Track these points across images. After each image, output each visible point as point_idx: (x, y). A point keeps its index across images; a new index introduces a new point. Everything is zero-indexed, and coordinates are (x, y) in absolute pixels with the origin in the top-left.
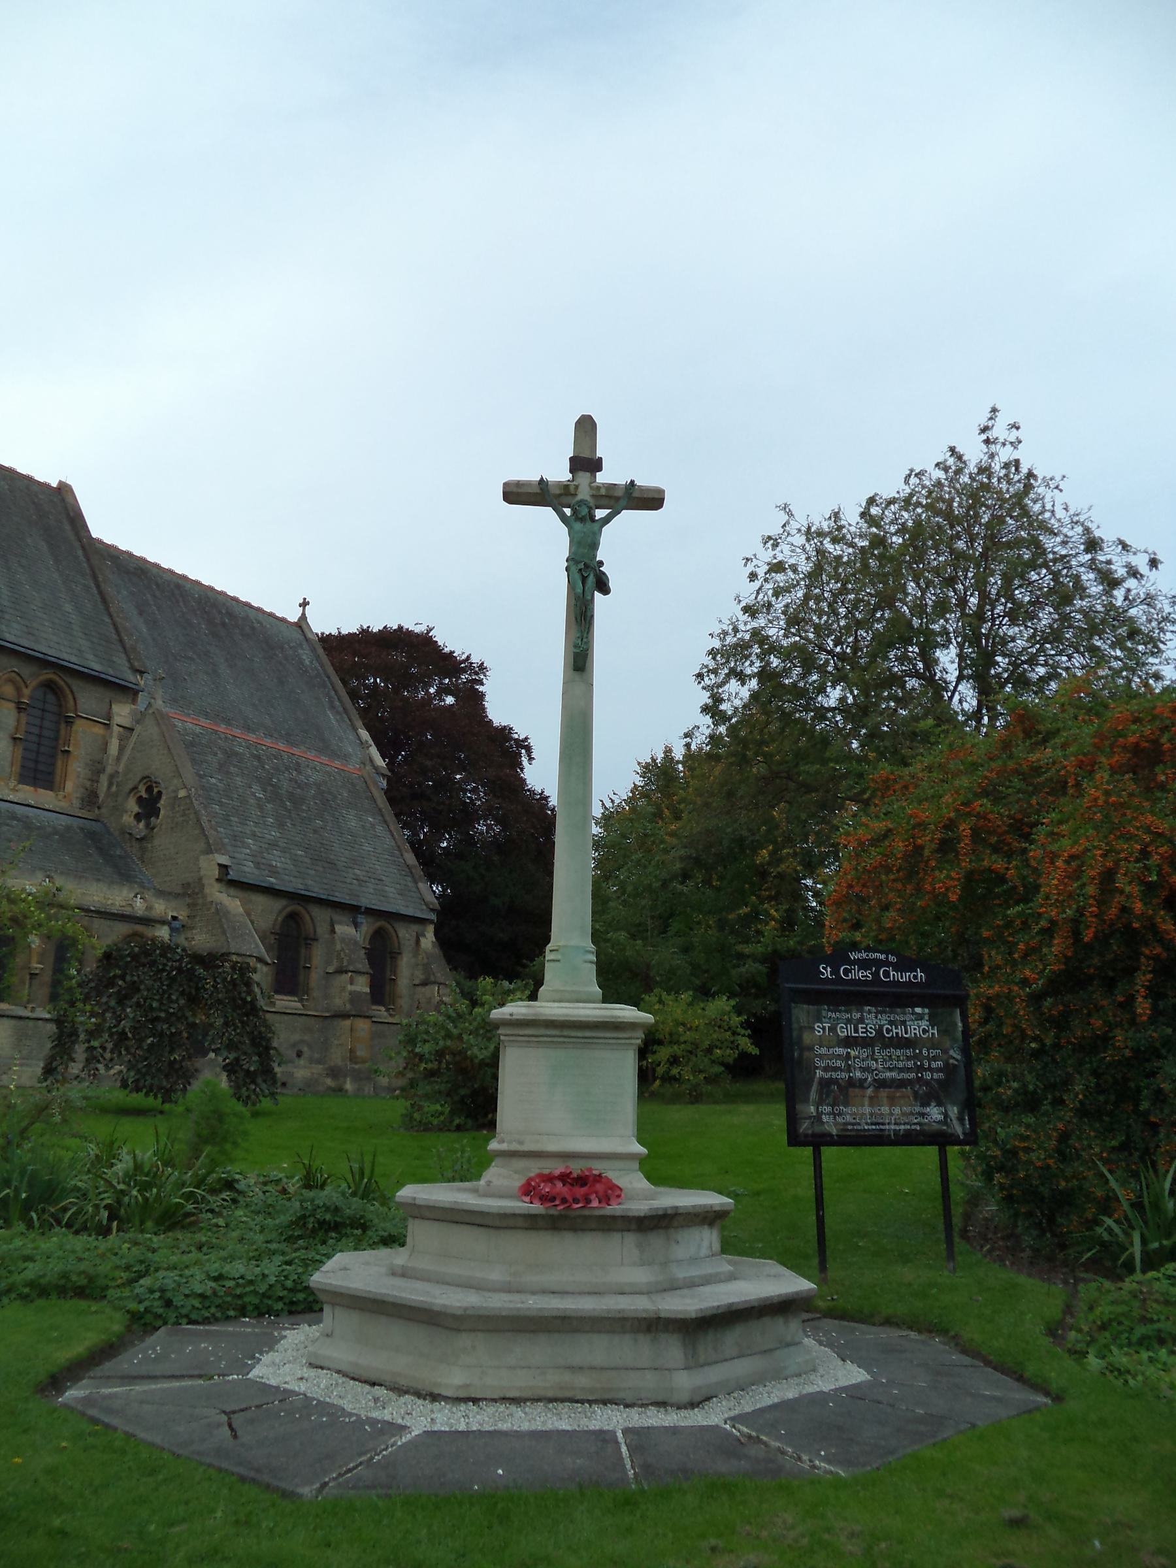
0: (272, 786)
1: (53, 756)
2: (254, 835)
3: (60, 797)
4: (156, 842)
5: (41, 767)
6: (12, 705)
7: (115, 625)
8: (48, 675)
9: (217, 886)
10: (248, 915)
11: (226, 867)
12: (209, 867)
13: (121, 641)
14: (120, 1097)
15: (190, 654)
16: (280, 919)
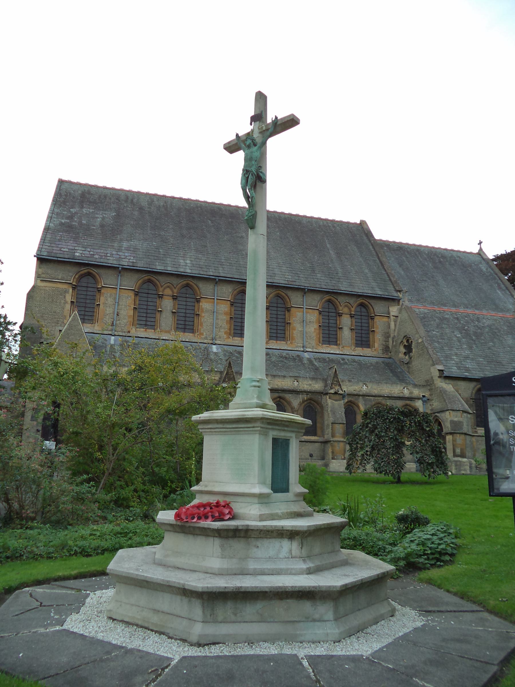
0: (465, 330)
2: (456, 354)
3: (373, 350)
4: (413, 363)
5: (364, 339)
6: (349, 316)
8: (360, 300)
9: (439, 380)
10: (457, 391)
11: (442, 370)
13: (390, 280)
14: (375, 476)
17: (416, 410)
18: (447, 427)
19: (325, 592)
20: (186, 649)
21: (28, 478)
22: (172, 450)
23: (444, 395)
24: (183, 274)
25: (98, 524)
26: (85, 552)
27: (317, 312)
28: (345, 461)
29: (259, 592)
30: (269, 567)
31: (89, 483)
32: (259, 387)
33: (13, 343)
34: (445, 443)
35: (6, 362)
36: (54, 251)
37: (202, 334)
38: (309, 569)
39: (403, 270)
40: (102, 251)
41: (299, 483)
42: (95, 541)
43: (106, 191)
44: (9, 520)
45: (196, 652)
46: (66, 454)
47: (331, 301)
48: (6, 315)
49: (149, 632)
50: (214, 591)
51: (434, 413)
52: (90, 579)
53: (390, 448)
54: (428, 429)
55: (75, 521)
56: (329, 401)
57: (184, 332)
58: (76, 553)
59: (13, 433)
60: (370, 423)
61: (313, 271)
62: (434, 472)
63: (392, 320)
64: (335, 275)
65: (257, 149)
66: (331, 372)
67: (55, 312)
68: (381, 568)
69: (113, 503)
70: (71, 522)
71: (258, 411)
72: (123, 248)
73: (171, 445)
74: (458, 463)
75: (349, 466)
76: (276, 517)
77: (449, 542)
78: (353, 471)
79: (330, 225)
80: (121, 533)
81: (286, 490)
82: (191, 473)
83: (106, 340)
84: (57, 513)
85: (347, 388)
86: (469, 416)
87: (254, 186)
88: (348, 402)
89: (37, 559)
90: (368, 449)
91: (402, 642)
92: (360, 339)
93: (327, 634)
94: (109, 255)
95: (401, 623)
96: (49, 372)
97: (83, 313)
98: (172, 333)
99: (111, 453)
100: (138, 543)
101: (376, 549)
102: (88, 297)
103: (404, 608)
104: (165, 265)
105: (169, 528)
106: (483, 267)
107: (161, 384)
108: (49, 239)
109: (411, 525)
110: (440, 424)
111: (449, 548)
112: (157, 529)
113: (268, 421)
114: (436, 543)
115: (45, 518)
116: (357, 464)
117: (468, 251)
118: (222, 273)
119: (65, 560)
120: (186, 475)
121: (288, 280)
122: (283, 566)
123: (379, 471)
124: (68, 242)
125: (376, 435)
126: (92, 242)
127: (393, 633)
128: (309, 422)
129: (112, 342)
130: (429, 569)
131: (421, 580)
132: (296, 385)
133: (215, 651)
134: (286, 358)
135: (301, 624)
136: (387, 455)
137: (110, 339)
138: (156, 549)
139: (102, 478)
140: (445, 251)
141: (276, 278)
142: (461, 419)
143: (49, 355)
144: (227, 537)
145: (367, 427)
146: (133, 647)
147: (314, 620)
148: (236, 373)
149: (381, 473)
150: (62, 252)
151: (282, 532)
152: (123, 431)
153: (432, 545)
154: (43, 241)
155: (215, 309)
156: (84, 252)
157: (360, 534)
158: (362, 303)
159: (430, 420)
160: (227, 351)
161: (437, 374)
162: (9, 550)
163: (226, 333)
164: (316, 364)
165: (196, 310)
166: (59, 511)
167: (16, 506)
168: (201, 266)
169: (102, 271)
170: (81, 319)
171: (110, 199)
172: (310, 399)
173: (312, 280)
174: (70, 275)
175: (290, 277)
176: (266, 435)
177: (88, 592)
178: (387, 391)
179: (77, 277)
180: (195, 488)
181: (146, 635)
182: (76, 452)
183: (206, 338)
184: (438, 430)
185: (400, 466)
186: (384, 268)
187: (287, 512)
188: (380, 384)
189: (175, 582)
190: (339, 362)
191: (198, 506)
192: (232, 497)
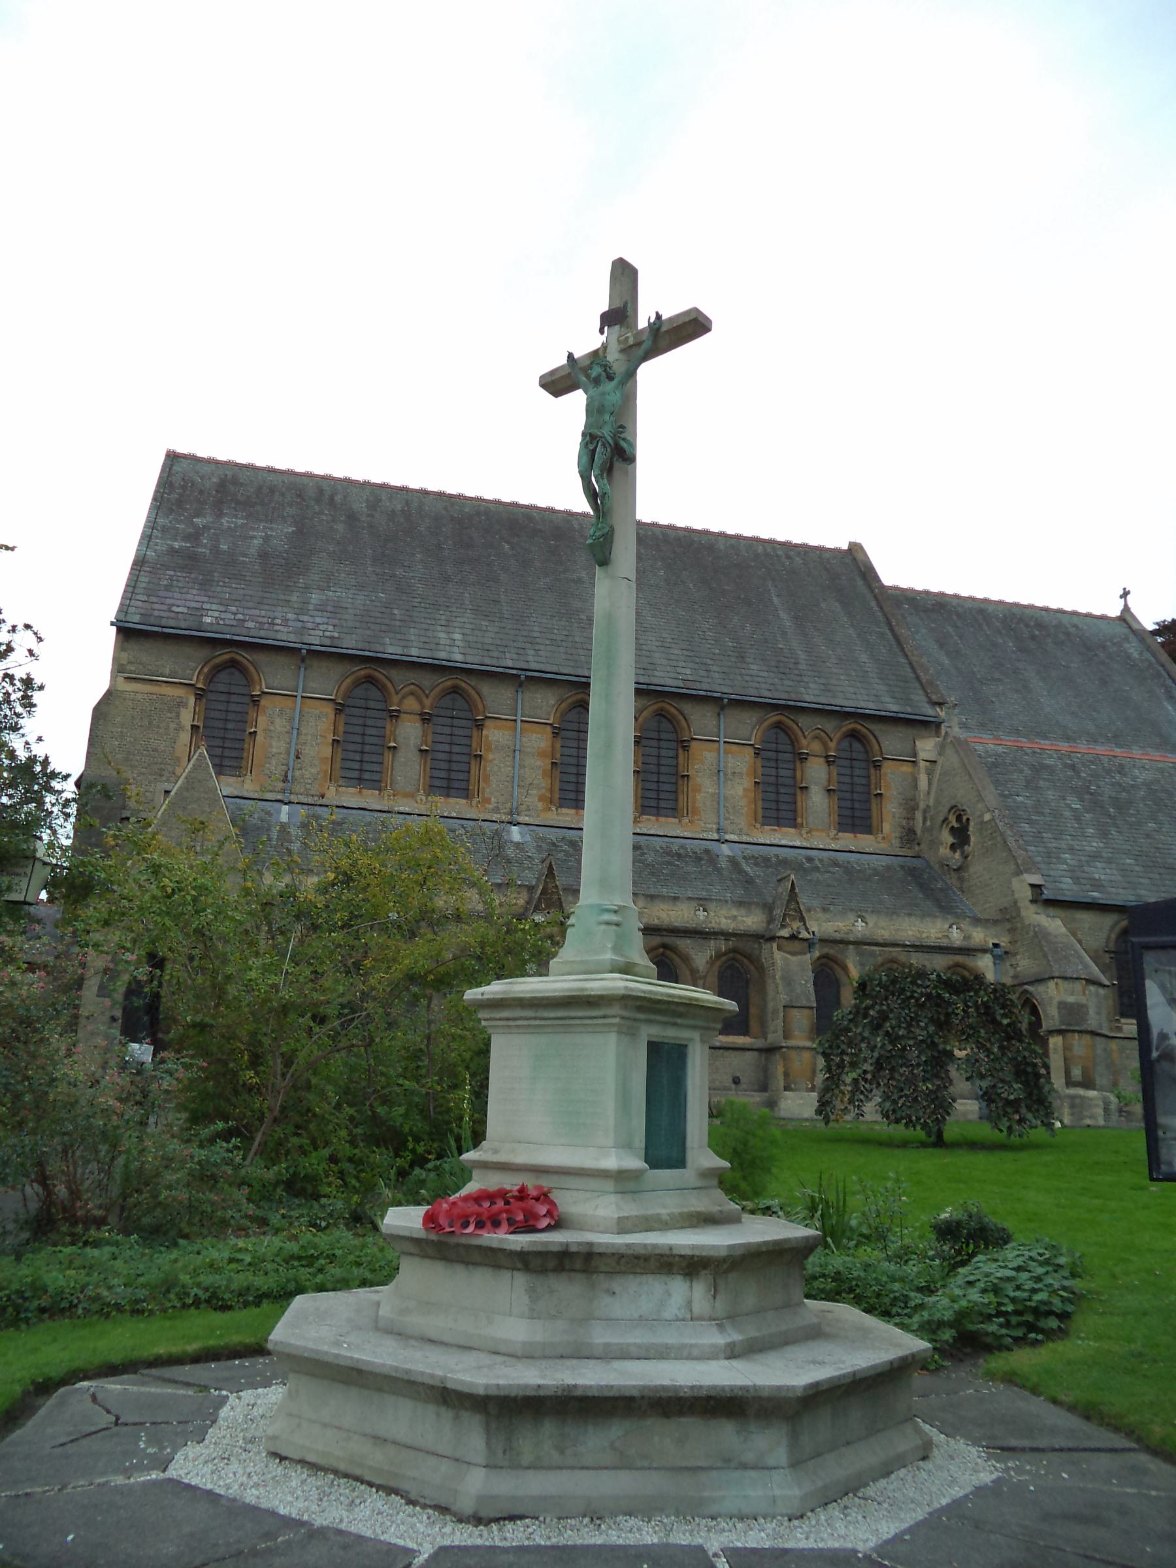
0: (1091, 794)
1: (868, 801)
2: (1071, 849)
3: (879, 839)
4: (971, 870)
6: (822, 760)
8: (849, 725)
10: (1074, 934)
11: (1039, 886)
13: (918, 678)
14: (884, 1129)
15: (997, 675)
16: (1113, 936)
17: (979, 978)
18: (1051, 1017)
19: (770, 1399)
20: (448, 1530)
22: (418, 1067)
23: (1044, 943)
24: (445, 663)
25: (247, 1236)
26: (218, 1299)
27: (751, 751)
28: (815, 1095)
30: (638, 1341)
31: (228, 1142)
32: (617, 925)
33: (61, 821)
34: (1046, 1054)
35: (45, 864)
36: (156, 613)
37: (488, 801)
42: (241, 1276)
45: (470, 1536)
46: (177, 1074)
47: (781, 725)
48: (47, 758)
49: (363, 1487)
50: (513, 1394)
52: (229, 1363)
54: (1005, 1022)
55: (195, 1229)
56: (778, 955)
57: (448, 796)
58: (197, 1303)
59: (58, 1025)
60: (872, 1007)
61: (742, 658)
62: (1021, 1121)
63: (922, 770)
64: (791, 666)
65: (617, 387)
66: (782, 889)
67: (155, 750)
68: (898, 1345)
69: (282, 1187)
70: (187, 1230)
72: (311, 607)
73: (417, 1055)
74: (1078, 1101)
75: (824, 1107)
78: (832, 1117)
79: (780, 553)
80: (300, 1258)
82: (461, 1118)
83: (269, 814)
84: (155, 1207)
85: (820, 925)
86: (1102, 991)
87: (608, 470)
89: (108, 1316)
91: (948, 1519)
92: (848, 813)
93: (774, 1500)
94: (278, 621)
96: (140, 886)
97: (218, 751)
99: (279, 1072)
100: (338, 1281)
101: (887, 1300)
103: (952, 1441)
105: (411, 1248)
106: (1133, 649)
107: (393, 916)
108: (144, 585)
109: (968, 1246)
110: (1034, 1011)
111: (1056, 1301)
112: (382, 1250)
113: (639, 1003)
114: (1026, 1287)
115: (127, 1219)
116: (842, 1101)
122: (668, 1337)
123: (892, 1117)
124: (187, 593)
126: (241, 592)
127: (927, 1498)
128: (731, 1005)
129: (284, 818)
130: (1009, 1349)
131: (991, 1376)
133: (514, 1535)
134: (679, 855)
135: (714, 1474)
136: (911, 1081)
137: (279, 812)
139: (257, 1130)
141: (657, 673)
142: (1083, 1000)
143: (141, 848)
144: (543, 1271)
145: (865, 1016)
146: (325, 1523)
147: (744, 1466)
148: (564, 889)
149: (897, 1121)
150: (173, 615)
151: (671, 1259)
152: (307, 1021)
154: (131, 589)
155: (518, 743)
156: (223, 616)
158: (854, 730)
160: (543, 839)
161: (1028, 893)
164: (748, 869)
165: (474, 745)
166: (160, 1203)
167: (61, 1190)
168: (486, 647)
169: (261, 658)
170: (214, 765)
171: (283, 495)
172: (735, 950)
173: (739, 678)
174: (191, 666)
175: (688, 671)
177: (224, 1393)
178: (910, 933)
179: (206, 670)
180: (470, 1156)
182: (201, 1068)
183: (496, 810)
185: (942, 1105)
186: (903, 650)
187: (680, 1214)
188: (894, 917)
189: (422, 1373)
190: (801, 865)
191: (478, 1198)
192: (555, 1178)
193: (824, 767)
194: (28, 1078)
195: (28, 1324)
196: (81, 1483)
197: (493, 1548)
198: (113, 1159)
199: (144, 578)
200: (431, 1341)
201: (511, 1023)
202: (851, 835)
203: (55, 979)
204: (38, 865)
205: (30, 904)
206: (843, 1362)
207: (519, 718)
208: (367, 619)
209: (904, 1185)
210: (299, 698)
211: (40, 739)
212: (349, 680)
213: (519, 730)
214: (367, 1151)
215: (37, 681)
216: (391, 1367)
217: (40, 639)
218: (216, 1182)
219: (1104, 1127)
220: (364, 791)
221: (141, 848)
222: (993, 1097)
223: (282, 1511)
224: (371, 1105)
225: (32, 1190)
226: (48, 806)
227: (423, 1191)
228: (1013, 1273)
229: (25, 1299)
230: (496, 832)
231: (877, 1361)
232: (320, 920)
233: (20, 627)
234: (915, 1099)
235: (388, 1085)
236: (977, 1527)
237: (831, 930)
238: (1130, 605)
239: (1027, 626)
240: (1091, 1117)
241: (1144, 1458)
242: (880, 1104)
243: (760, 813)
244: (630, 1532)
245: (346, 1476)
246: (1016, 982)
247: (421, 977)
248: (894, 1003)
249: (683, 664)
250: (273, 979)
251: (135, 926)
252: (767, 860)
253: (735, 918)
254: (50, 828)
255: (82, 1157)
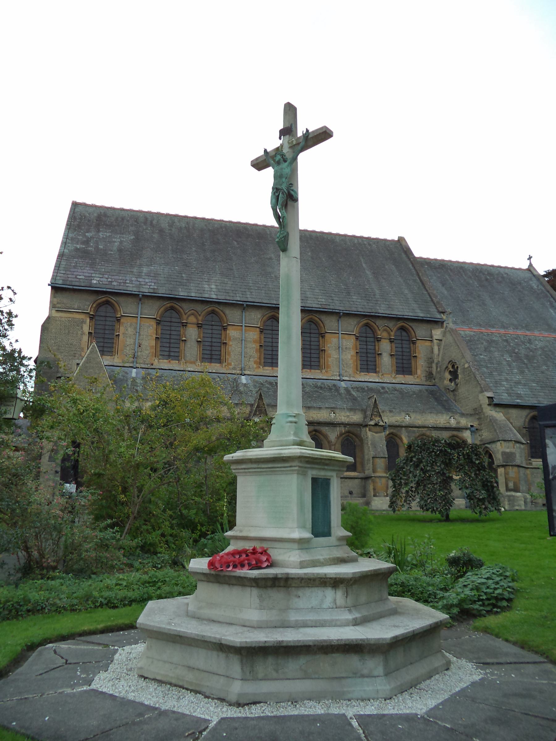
0: (516, 353)
1: (410, 359)
2: (507, 380)
4: (460, 391)
5: (405, 365)
6: (388, 341)
7: (429, 294)
8: (400, 324)
9: (489, 408)
10: (509, 420)
11: (492, 398)
12: (483, 399)
13: (432, 300)
14: (421, 514)
16: (527, 420)
17: (464, 442)
18: (498, 459)
19: (374, 645)
20: (225, 709)
21: (48, 524)
22: (201, 491)
24: (208, 299)
25: (124, 572)
26: (111, 603)
27: (354, 337)
28: (388, 498)
29: (301, 646)
30: (311, 618)
31: (113, 529)
32: (295, 423)
33: (28, 379)
34: (497, 477)
35: (22, 400)
36: (70, 279)
37: (231, 364)
38: (355, 619)
39: (446, 289)
40: (121, 278)
41: (342, 526)
42: (122, 592)
43: (123, 213)
44: (29, 570)
45: (235, 712)
46: (88, 497)
47: (368, 325)
48: (20, 350)
49: (184, 691)
50: (253, 645)
51: (484, 444)
52: (118, 633)
53: (437, 483)
54: (477, 462)
55: (99, 570)
56: (369, 434)
57: (211, 362)
58: (101, 605)
59: (31, 477)
60: (415, 457)
61: (348, 293)
62: (486, 508)
63: (435, 344)
64: (372, 296)
65: (288, 166)
66: (370, 402)
67: (71, 344)
68: (433, 617)
69: (139, 549)
70: (95, 571)
71: (295, 449)
72: (143, 274)
73: (200, 485)
74: (512, 498)
75: (392, 504)
76: (318, 564)
77: (506, 586)
78: (397, 509)
79: (365, 243)
80: (149, 583)
81: (328, 534)
82: (222, 515)
83: (126, 373)
84: (79, 561)
85: (388, 419)
86: (522, 446)
87: (285, 206)
88: (389, 434)
89: (60, 612)
90: (413, 485)
91: (459, 698)
92: (401, 365)
93: (378, 691)
94: (128, 282)
95: (457, 677)
96: (67, 410)
97: (102, 344)
98: (197, 364)
99: (136, 495)
100: (167, 593)
101: (426, 595)
102: (107, 327)
103: (460, 661)
104: (189, 291)
105: (203, 578)
106: (534, 284)
107: (188, 420)
108: (63, 266)
109: (463, 568)
110: (490, 456)
111: (506, 593)
112: (188, 577)
113: (307, 460)
114: (492, 587)
115: (67, 566)
116: (401, 501)
117: (516, 267)
118: (251, 297)
119: (90, 613)
120: (216, 517)
121: (322, 303)
122: (326, 616)
123: (425, 508)
124: (84, 269)
125: (422, 469)
126: (110, 268)
127: (449, 688)
128: (350, 459)
129: (134, 375)
130: (485, 616)
131: (476, 629)
132: (333, 417)
133: (256, 711)
134: (321, 388)
135: (349, 680)
136: (434, 491)
137: (131, 372)
138: (189, 599)
139: (127, 523)
140: (491, 268)
141: (308, 302)
142: (513, 450)
143: (67, 391)
144: (266, 587)
145: (411, 461)
146: (167, 708)
147: (363, 676)
148: (268, 405)
149: (427, 510)
150: (78, 280)
151: (325, 580)
152: (148, 470)
153: (488, 590)
154: (57, 268)
155: (244, 336)
156: (102, 279)
157: (408, 579)
158: (402, 326)
159: (479, 452)
160: (257, 382)
161: (487, 401)
162: (30, 602)
163: (255, 362)
164: (354, 393)
165: (223, 338)
166: (82, 559)
167: (35, 554)
168: (227, 291)
169: (121, 299)
170: (100, 351)
171: (128, 221)
172: (349, 432)
173: (347, 303)
174: (87, 304)
175: (323, 300)
176: (304, 474)
177: (116, 648)
178: (431, 421)
179: (94, 306)
180: (229, 533)
181: (180, 694)
182: (99, 495)
183: (234, 369)
184: (489, 463)
185: (448, 502)
186: (425, 288)
187: (329, 558)
188: (424, 414)
189: (210, 637)
190: (379, 391)
191: (233, 553)
192: (269, 543)
193: (389, 344)
194: (18, 502)
195: (22, 617)
196: (51, 692)
197: (246, 718)
198: (59, 538)
199: (63, 263)
200: (214, 621)
201: (246, 471)
202: (402, 376)
203: (29, 454)
204: (18, 401)
205: (15, 419)
206: (408, 626)
207: (244, 325)
208: (170, 279)
209: (433, 540)
210: (139, 318)
211: (17, 341)
212: (162, 309)
213: (244, 330)
214: (179, 531)
215: (14, 313)
216: (195, 634)
217: (15, 293)
218: (108, 547)
219: (524, 510)
220: (172, 361)
221: (67, 391)
222: (473, 497)
223: (146, 703)
224: (180, 510)
225: (22, 554)
226: (22, 373)
227: (206, 549)
228: (484, 581)
229: (21, 606)
230: (235, 379)
231: (424, 625)
232: (153, 423)
233: (5, 288)
234: (436, 500)
235: (188, 500)
236: (473, 701)
237: (394, 421)
238: (532, 263)
239: (484, 274)
240: (518, 506)
241: (550, 666)
242: (419, 502)
243: (359, 366)
244: (311, 708)
245: (175, 685)
246: (482, 443)
247: (201, 449)
248: (425, 454)
249: (321, 297)
250: (131, 451)
251: (65, 428)
252: (363, 389)
253: (348, 416)
254: (23, 383)
255: (44, 538)
